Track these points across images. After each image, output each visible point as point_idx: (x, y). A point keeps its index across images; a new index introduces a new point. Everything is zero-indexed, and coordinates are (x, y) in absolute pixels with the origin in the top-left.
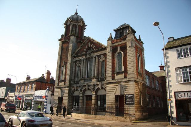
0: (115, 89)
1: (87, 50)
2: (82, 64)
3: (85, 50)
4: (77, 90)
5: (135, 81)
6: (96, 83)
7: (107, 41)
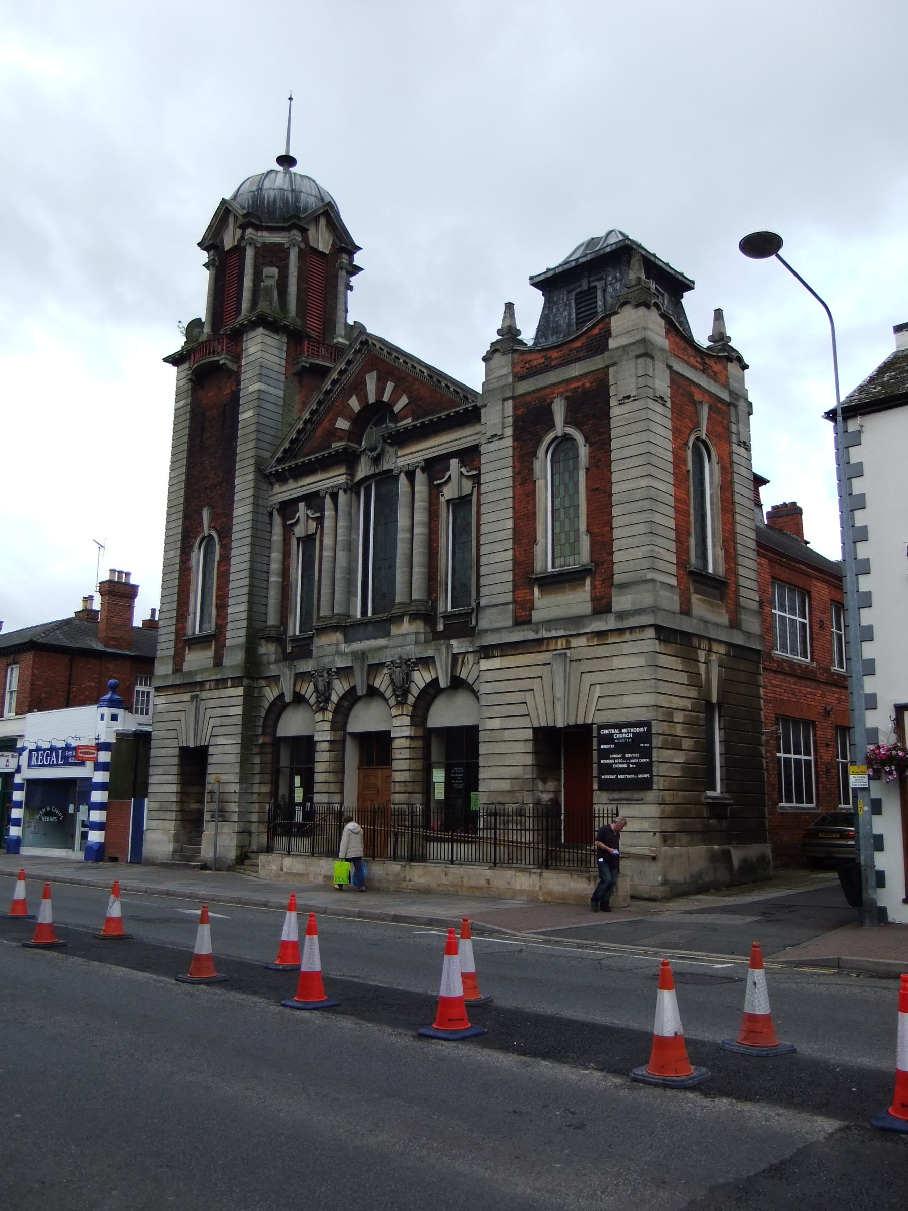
0: (545, 671)
1: (360, 422)
2: (328, 523)
3: (342, 424)
4: (299, 699)
5: (664, 634)
6: (414, 652)
7: (485, 359)
